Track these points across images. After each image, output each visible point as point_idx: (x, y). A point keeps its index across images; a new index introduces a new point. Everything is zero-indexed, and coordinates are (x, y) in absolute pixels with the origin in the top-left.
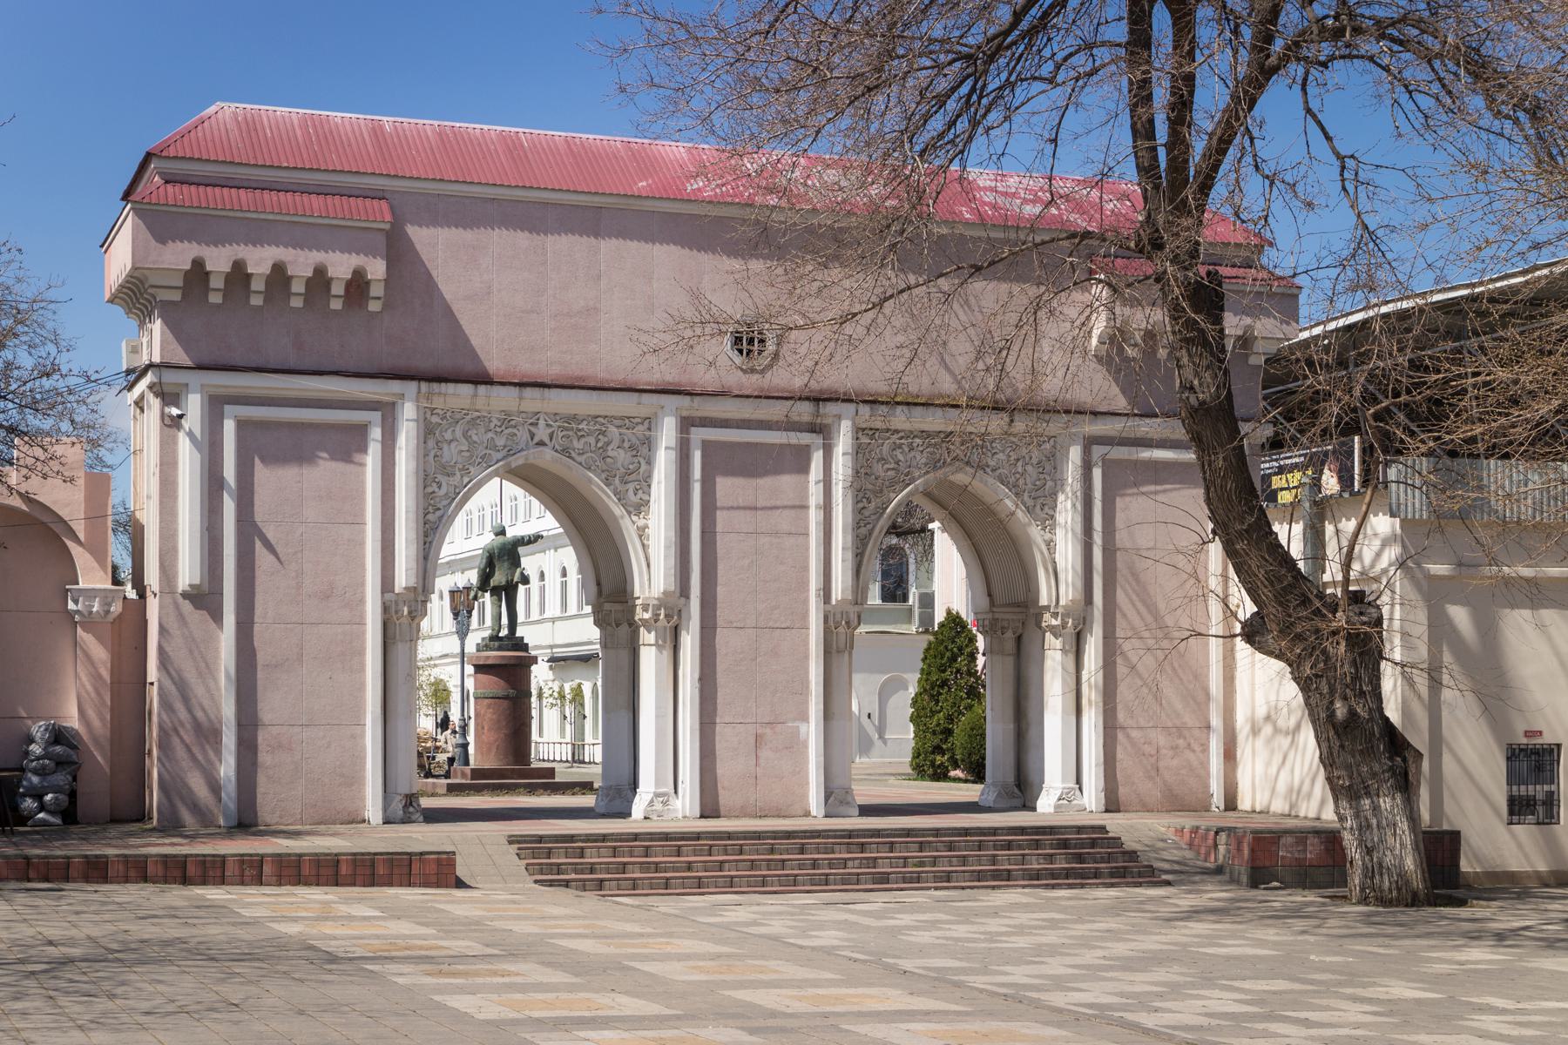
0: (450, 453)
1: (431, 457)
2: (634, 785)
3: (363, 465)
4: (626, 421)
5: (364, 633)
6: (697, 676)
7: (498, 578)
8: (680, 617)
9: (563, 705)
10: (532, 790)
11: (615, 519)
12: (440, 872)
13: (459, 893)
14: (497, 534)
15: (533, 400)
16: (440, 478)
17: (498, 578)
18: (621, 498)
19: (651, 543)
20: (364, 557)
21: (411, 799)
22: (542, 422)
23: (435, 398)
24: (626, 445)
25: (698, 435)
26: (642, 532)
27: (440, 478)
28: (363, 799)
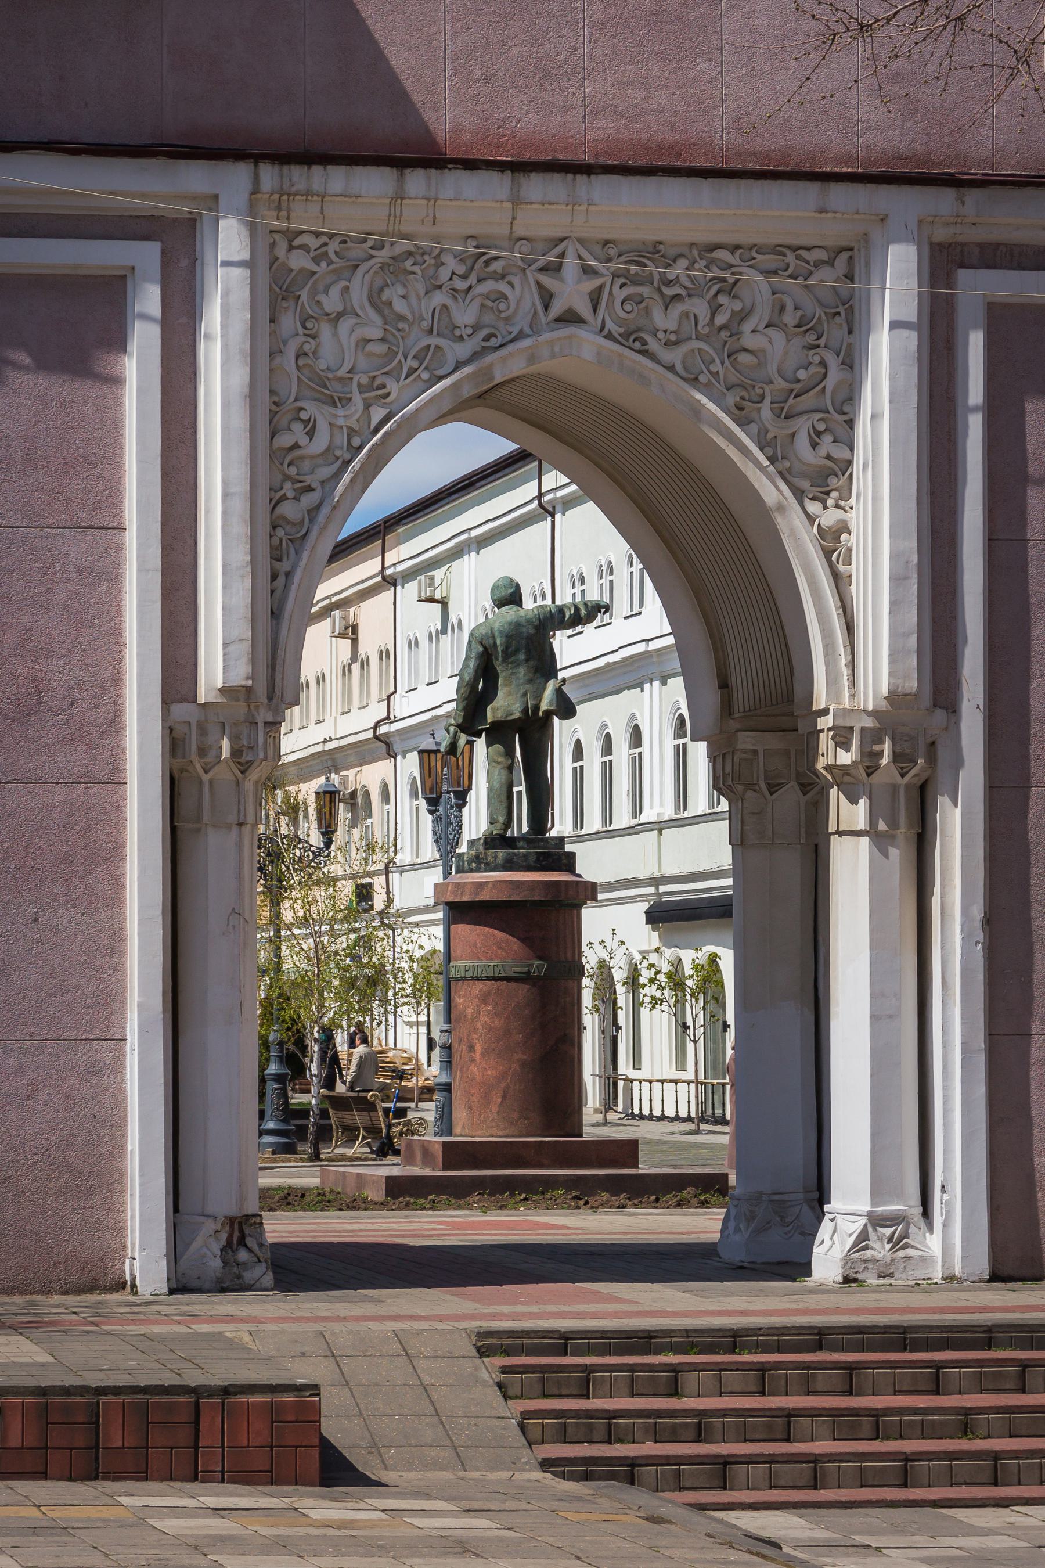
0: (337, 347)
1: (288, 360)
2: (819, 1192)
3: (116, 381)
4: (786, 257)
5: (119, 805)
6: (978, 912)
7: (506, 703)
8: (932, 760)
9: (680, 1003)
10: (583, 1193)
11: (764, 514)
12: (286, 1443)
13: (321, 1508)
14: (500, 603)
15: (548, 208)
16: (311, 409)
17: (506, 703)
18: (777, 453)
19: (857, 570)
20: (119, 611)
21: (242, 1229)
22: (570, 262)
23: (298, 207)
24: (790, 318)
25: (976, 287)
26: (831, 541)
27: (311, 409)
28: (120, 1231)
